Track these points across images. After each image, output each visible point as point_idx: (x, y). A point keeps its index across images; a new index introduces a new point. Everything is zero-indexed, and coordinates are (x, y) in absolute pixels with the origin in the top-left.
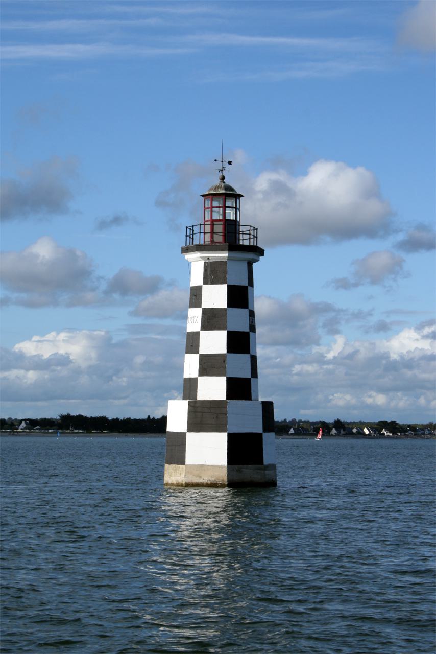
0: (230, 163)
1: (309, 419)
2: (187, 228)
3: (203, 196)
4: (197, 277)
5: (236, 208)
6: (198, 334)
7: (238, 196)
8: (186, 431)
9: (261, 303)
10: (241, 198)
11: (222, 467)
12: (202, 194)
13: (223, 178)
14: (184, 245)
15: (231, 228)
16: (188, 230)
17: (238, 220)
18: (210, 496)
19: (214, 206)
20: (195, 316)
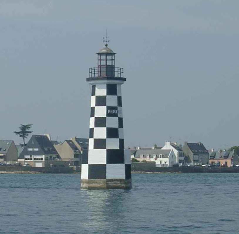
0: (108, 42)
1: (236, 145)
2: (90, 69)
3: (98, 54)
4: (93, 103)
5: (112, 59)
6: (94, 108)
7: (113, 54)
8: (124, 164)
9: (125, 111)
10: (115, 54)
11: (35, 166)
12: (98, 52)
13: (106, 45)
14: (88, 77)
15: (110, 69)
16: (91, 70)
17: (113, 64)
18: (76, 202)
19: (102, 58)
20: (92, 120)
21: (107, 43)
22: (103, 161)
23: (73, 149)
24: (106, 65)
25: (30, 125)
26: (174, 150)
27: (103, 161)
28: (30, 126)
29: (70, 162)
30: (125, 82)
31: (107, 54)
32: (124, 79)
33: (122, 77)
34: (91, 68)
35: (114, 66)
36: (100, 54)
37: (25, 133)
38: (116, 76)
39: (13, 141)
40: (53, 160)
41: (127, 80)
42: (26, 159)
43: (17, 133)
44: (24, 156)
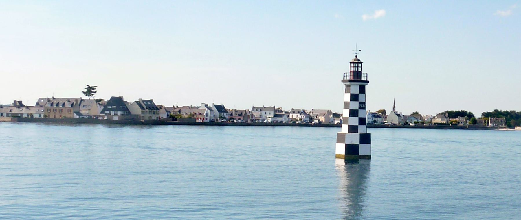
21: (357, 55)
22: (357, 124)
23: (141, 108)
24: (353, 71)
25: (95, 87)
26: (66, 104)
27: (357, 124)
28: (94, 88)
29: (341, 123)
30: (368, 84)
31: (358, 63)
32: (368, 82)
33: (364, 80)
34: (346, 72)
35: (361, 72)
36: (351, 63)
37: (91, 93)
38: (362, 79)
39: (135, 101)
40: (299, 121)
41: (370, 82)
42: (106, 114)
43: (84, 92)
44: (104, 112)
